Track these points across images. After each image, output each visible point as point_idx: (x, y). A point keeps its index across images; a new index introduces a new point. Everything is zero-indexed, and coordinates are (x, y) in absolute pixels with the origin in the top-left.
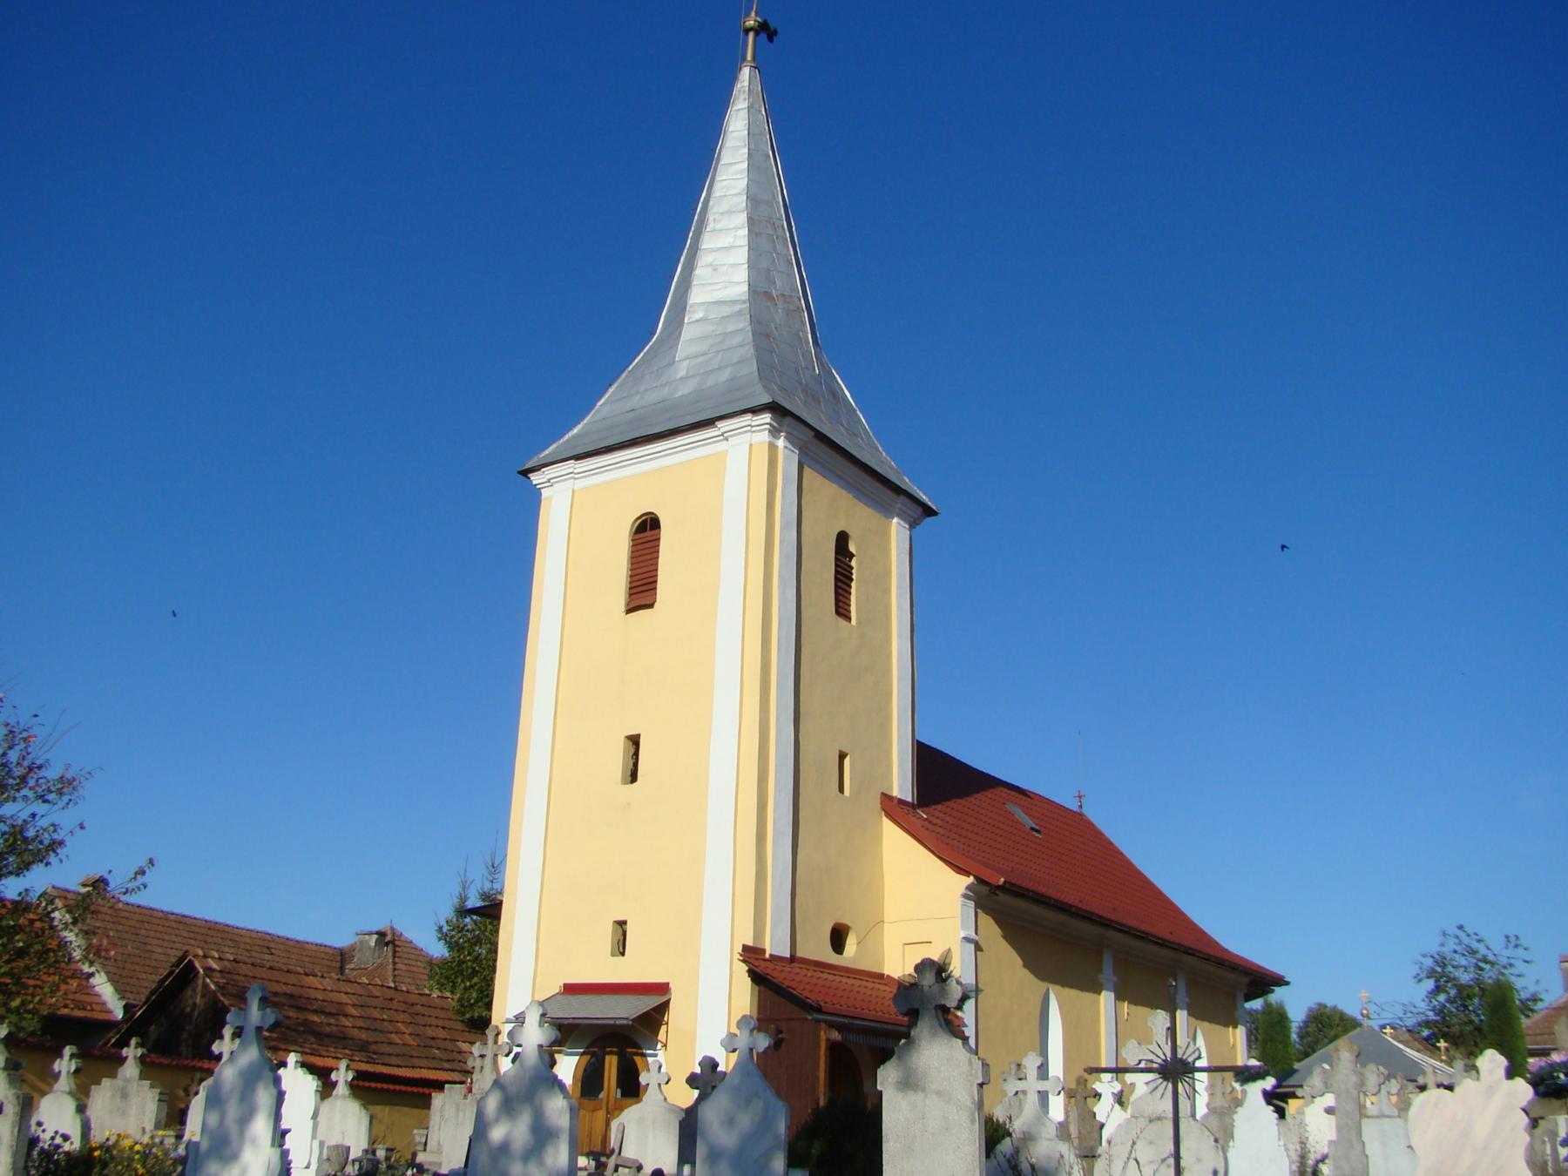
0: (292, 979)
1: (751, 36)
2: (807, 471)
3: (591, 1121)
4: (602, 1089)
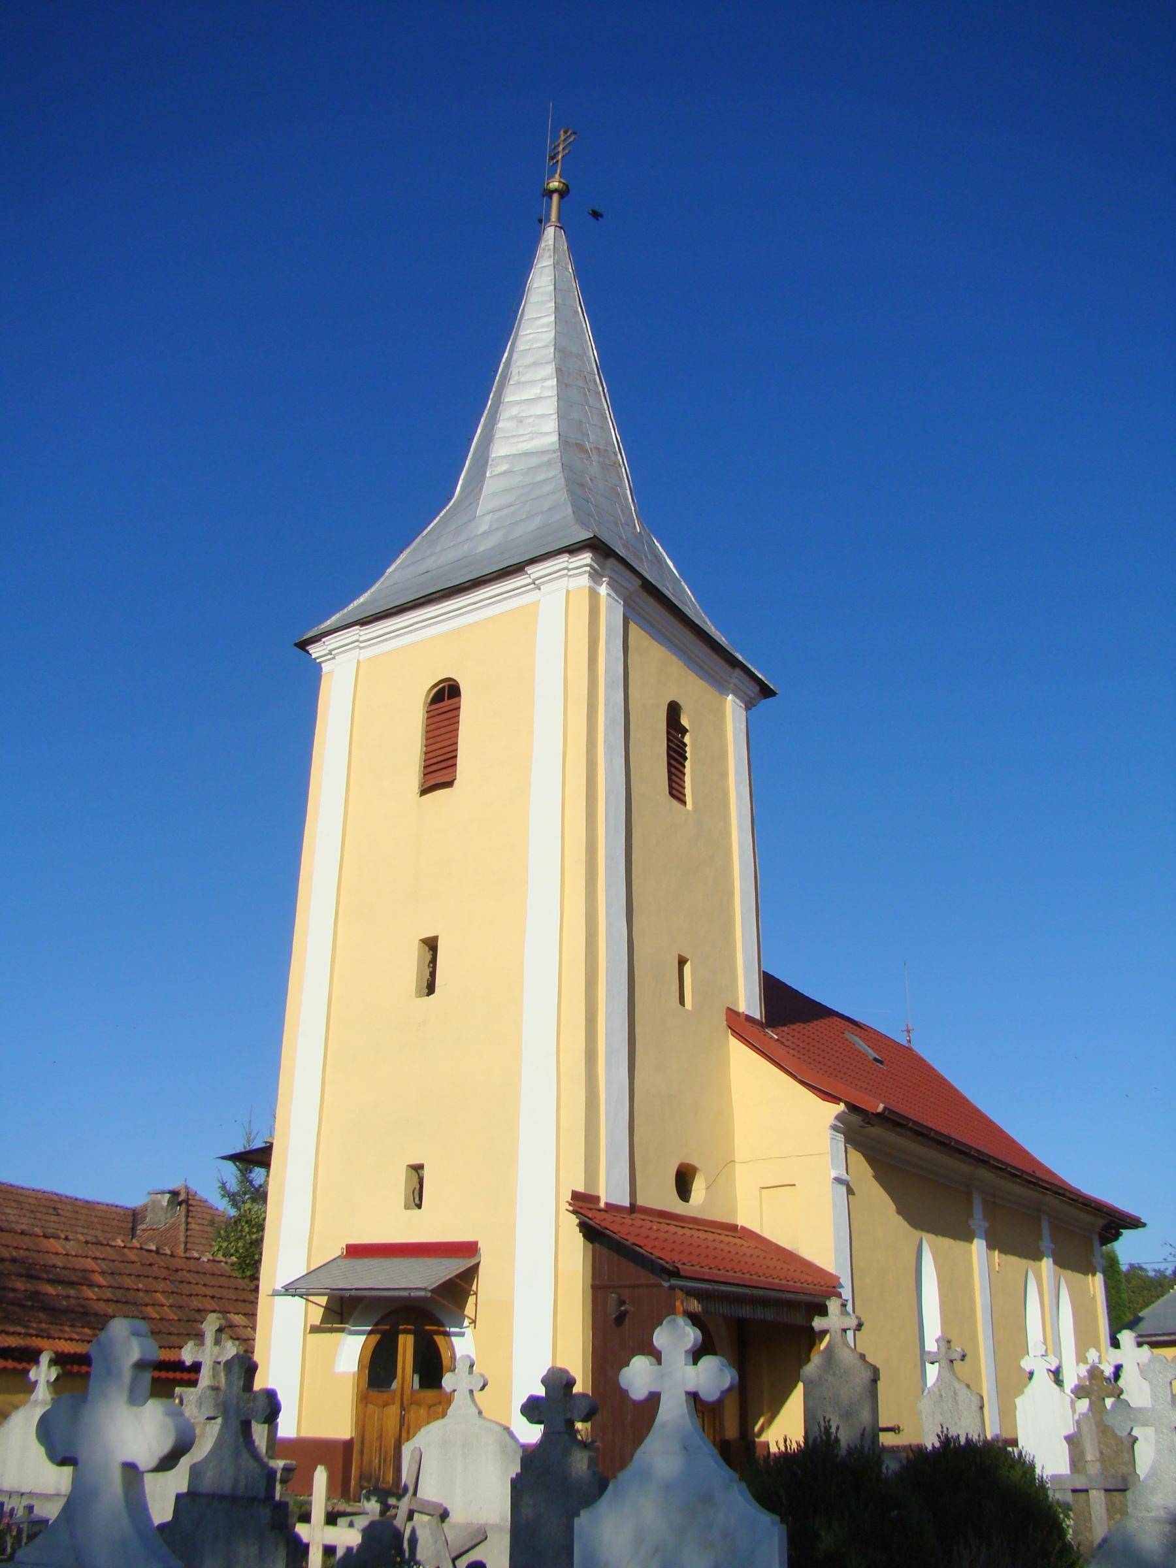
0: (26, 1241)
1: (555, 197)
2: (633, 627)
3: (381, 1419)
4: (394, 1376)
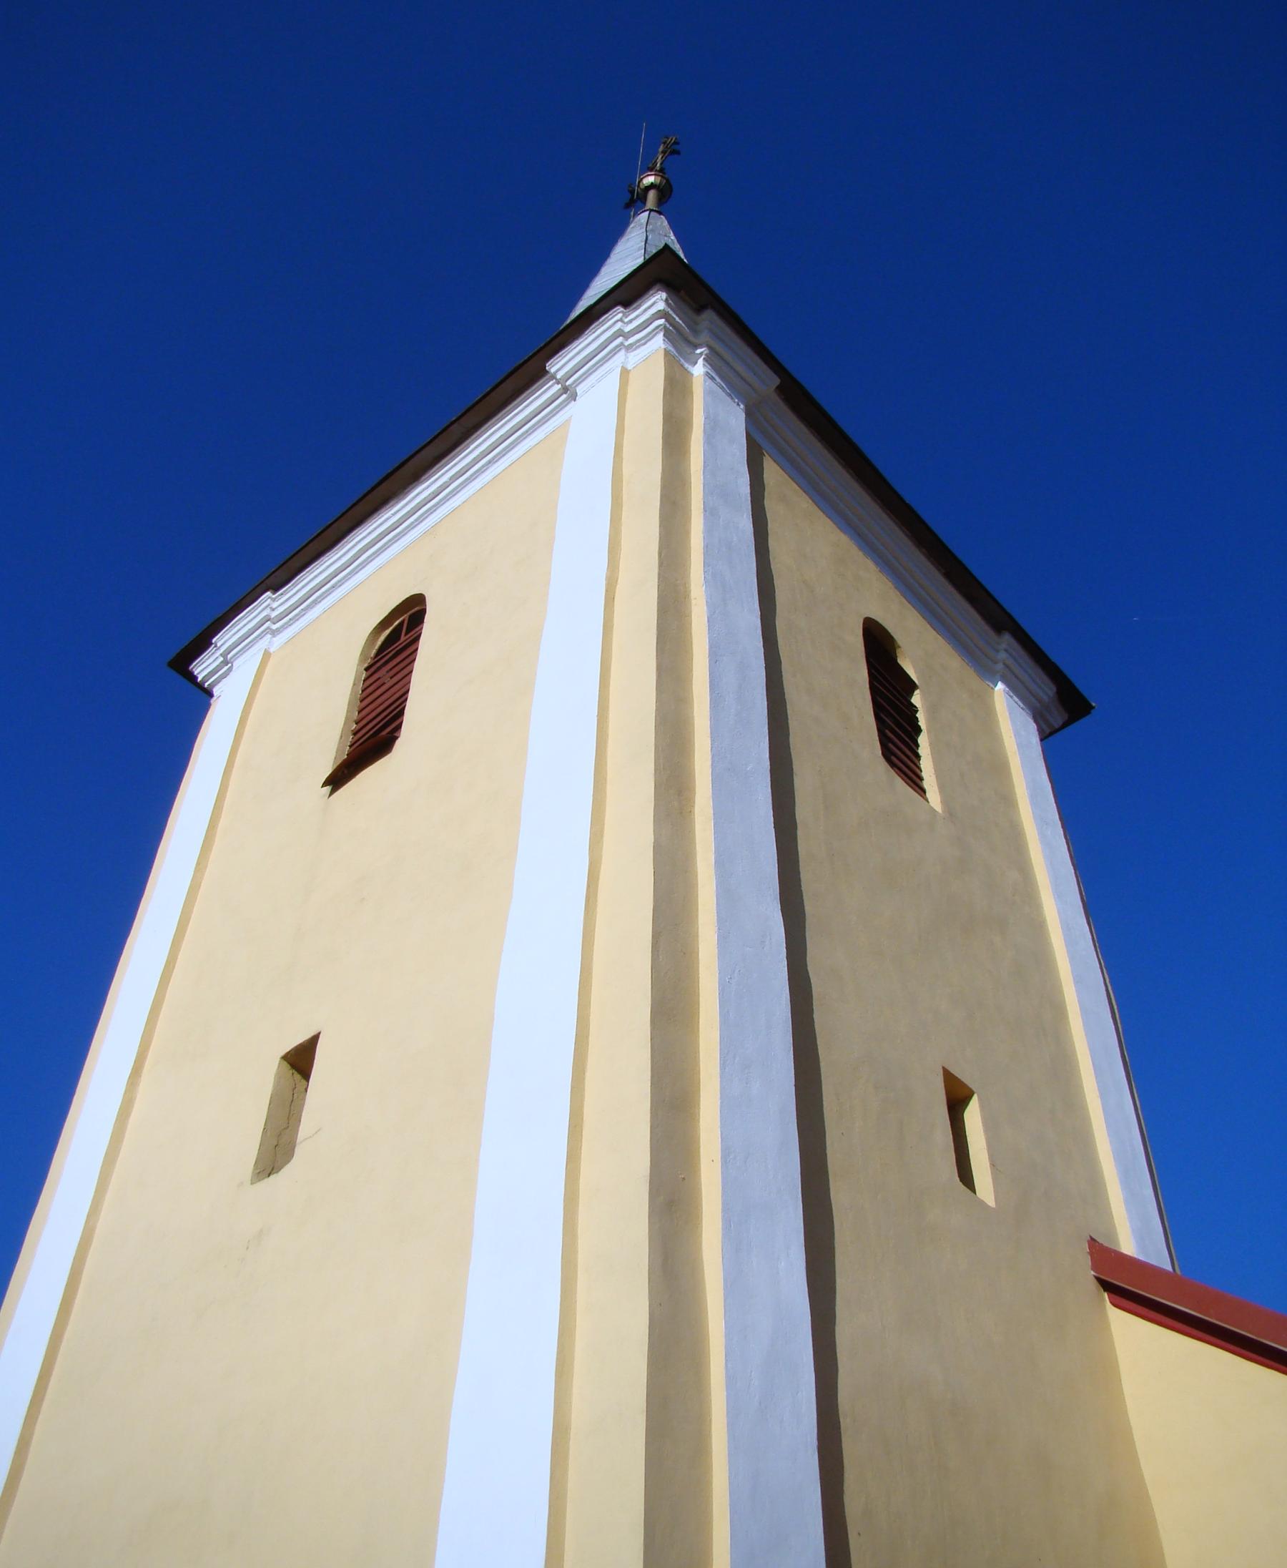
2: (772, 472)
